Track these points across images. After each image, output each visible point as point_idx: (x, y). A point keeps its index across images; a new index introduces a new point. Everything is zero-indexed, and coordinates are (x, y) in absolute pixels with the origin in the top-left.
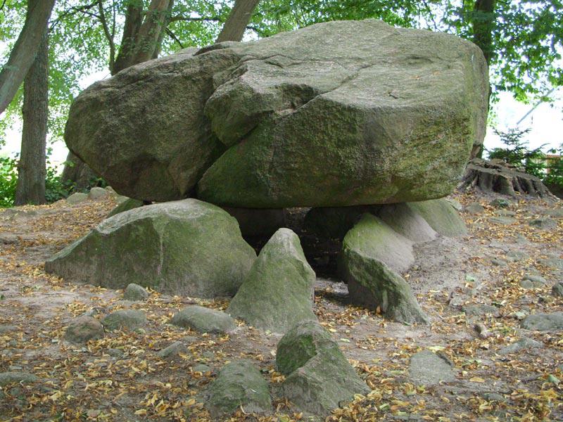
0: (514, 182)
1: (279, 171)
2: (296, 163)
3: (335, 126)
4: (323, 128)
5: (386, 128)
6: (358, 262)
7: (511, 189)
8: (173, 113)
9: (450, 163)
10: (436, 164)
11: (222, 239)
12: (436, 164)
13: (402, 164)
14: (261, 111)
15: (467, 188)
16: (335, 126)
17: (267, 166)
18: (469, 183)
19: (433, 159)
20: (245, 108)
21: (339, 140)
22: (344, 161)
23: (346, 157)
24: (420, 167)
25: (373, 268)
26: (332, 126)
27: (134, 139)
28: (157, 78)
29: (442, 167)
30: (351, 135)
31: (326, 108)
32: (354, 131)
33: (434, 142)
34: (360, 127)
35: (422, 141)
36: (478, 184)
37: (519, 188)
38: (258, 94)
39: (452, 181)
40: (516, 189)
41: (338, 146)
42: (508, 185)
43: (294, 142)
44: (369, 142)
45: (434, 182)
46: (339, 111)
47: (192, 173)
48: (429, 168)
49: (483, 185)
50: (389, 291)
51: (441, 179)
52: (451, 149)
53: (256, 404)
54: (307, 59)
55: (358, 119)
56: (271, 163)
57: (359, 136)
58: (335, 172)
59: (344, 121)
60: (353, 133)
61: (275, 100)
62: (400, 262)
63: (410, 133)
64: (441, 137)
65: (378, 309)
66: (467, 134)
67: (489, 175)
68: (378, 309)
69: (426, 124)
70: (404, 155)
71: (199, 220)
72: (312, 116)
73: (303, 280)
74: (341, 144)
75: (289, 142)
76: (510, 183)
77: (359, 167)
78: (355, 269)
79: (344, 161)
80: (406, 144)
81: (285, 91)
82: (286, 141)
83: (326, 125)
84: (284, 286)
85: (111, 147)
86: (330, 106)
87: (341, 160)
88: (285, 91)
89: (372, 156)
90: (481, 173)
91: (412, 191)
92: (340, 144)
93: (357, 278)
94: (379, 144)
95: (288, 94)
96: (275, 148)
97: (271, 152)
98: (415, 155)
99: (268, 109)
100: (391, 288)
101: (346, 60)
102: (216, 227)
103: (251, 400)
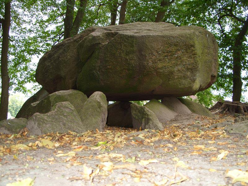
0: (244, 108)
1: (103, 71)
2: (110, 65)
3: (125, 45)
4: (120, 47)
5: (148, 44)
6: (135, 108)
7: (243, 111)
8: (68, 56)
9: (188, 69)
10: (180, 68)
11: (78, 103)
12: (180, 68)
13: (160, 65)
14: (94, 43)
15: (224, 112)
16: (125, 45)
17: (98, 68)
18: (225, 110)
19: (177, 65)
20: (88, 43)
21: (127, 52)
22: (129, 62)
23: (130, 59)
24: (170, 68)
25: (141, 110)
26: (124, 46)
27: (55, 70)
28: (66, 44)
29: (183, 70)
30: (132, 49)
31: (121, 38)
32: (132, 46)
33: (176, 56)
34: (135, 44)
35: (169, 54)
36: (228, 110)
37: (247, 111)
38: (94, 36)
39: (191, 79)
40: (245, 111)
41: (127, 55)
42: (241, 109)
43: (109, 55)
44: (140, 51)
45: (181, 78)
46: (126, 38)
47: (73, 80)
48: (176, 69)
49: (231, 110)
50: (145, 118)
51: (184, 76)
52: (186, 61)
53: (6, 129)
54: (125, 29)
55: (134, 41)
56: (99, 67)
57: (135, 49)
58: (126, 67)
59: (129, 43)
60: (132, 48)
61: (101, 38)
62: (166, 118)
63: (161, 48)
64: (180, 53)
65: (140, 128)
66: (195, 54)
67: (233, 106)
68: (140, 128)
69: (170, 45)
70: (160, 60)
71: (69, 95)
72: (115, 42)
73: (99, 110)
74: (128, 54)
75: (106, 56)
76: (242, 108)
77: (137, 64)
78: (134, 112)
79: (129, 62)
80: (160, 54)
81: (106, 35)
82: (105, 56)
83: (121, 46)
84: (89, 113)
85: (46, 75)
86: (123, 37)
87: (128, 61)
88: (106, 35)
89: (142, 58)
90: (229, 105)
91: (169, 82)
92: (127, 53)
93: (134, 116)
94: (145, 52)
95: (108, 37)
96: (101, 59)
97: (99, 61)
98: (166, 61)
99: (97, 42)
100: (147, 117)
101: (143, 30)
102: (76, 98)
103: (3, 126)
